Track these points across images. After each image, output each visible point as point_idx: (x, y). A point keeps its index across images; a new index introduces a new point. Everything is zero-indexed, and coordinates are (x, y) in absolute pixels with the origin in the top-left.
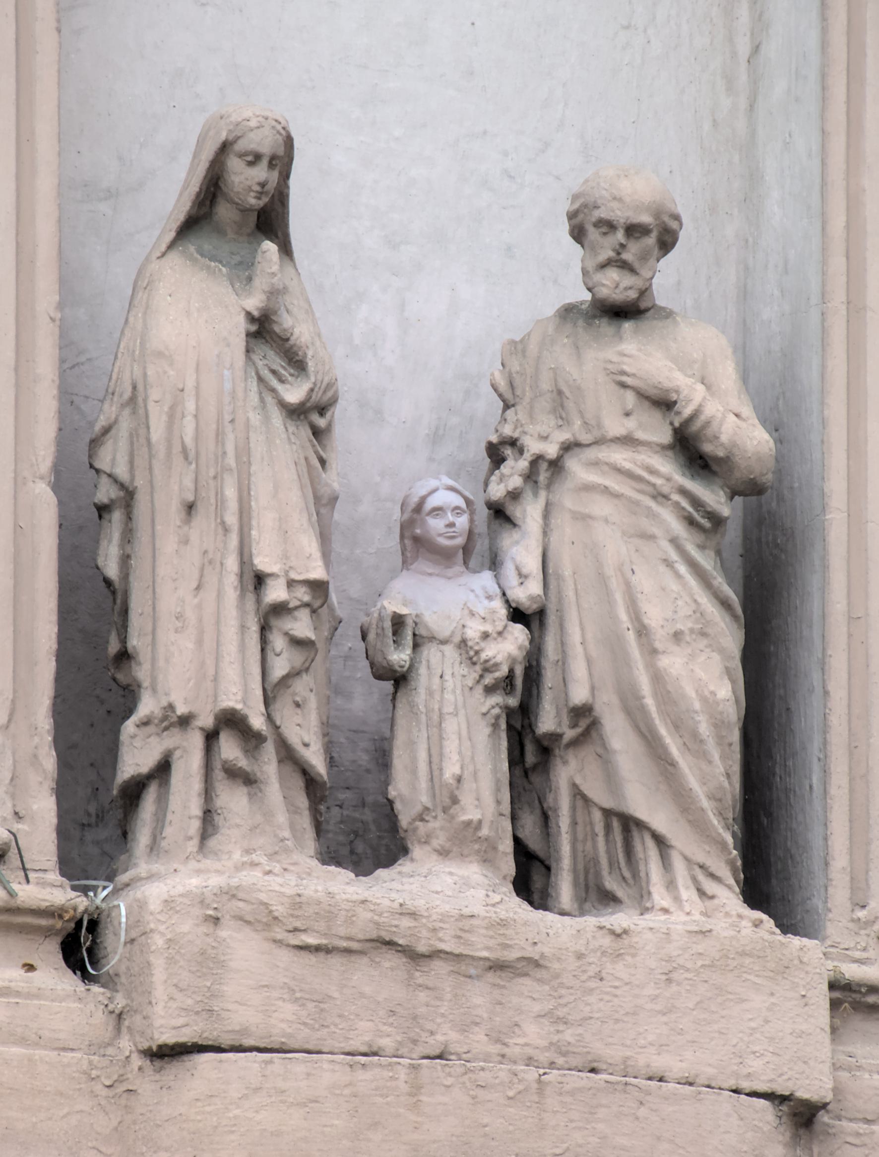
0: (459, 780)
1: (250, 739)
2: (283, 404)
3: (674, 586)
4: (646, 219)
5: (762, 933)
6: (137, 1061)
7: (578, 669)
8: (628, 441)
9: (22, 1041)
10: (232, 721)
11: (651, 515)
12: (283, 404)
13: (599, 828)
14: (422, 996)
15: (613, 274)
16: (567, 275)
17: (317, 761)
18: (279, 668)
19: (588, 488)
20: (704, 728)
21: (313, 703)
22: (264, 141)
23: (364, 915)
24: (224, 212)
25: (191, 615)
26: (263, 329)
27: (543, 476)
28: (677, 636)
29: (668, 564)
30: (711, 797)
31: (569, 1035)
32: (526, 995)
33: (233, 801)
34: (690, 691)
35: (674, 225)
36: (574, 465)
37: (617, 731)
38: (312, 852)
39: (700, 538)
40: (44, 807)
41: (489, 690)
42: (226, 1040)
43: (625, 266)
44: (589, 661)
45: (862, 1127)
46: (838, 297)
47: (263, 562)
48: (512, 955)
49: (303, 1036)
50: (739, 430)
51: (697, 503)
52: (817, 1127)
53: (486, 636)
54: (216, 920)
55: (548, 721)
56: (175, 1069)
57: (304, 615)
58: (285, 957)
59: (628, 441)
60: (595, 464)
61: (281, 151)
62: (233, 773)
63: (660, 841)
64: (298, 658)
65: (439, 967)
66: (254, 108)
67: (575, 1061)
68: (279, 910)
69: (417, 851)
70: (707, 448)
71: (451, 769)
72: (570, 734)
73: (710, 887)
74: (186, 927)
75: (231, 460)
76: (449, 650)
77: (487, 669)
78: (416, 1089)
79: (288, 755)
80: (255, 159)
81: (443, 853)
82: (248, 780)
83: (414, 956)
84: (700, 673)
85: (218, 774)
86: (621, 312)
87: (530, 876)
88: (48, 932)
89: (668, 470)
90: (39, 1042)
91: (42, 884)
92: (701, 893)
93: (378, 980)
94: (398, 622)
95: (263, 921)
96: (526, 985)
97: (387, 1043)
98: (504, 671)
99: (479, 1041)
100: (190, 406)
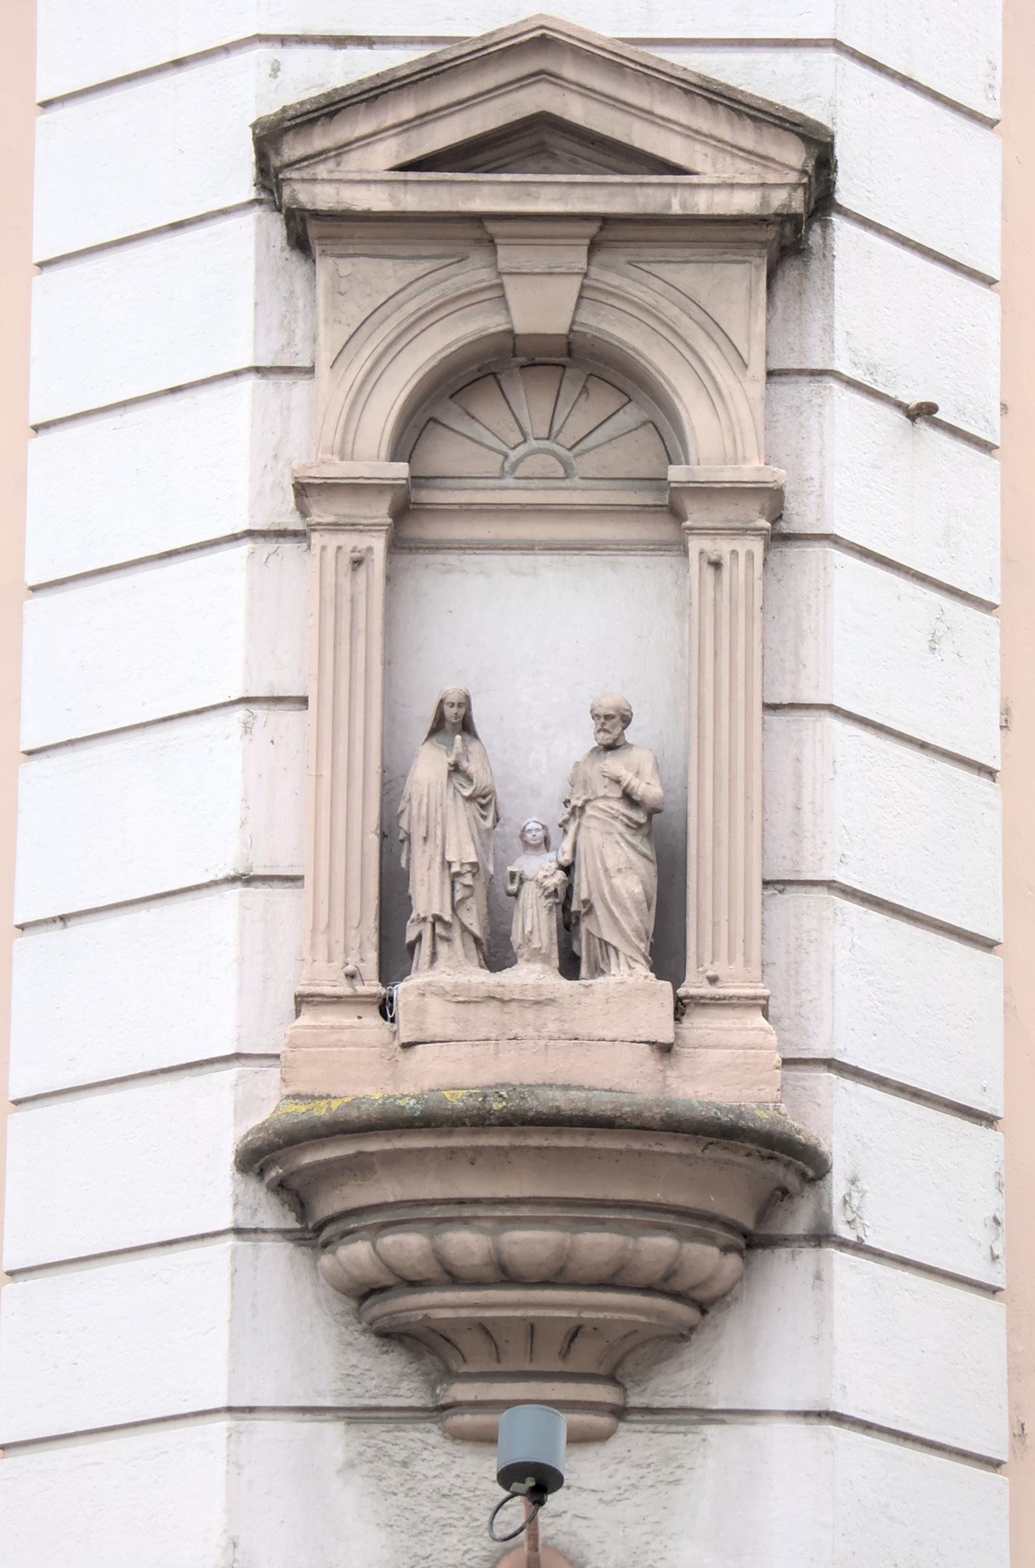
0: (531, 933)
1: (447, 925)
2: (463, 797)
3: (619, 851)
4: (611, 712)
5: (648, 981)
6: (399, 1049)
7: (584, 886)
8: (605, 797)
9: (356, 1045)
10: (438, 919)
11: (611, 825)
12: (463, 797)
13: (598, 945)
14: (507, 1016)
15: (602, 734)
16: (586, 737)
17: (477, 931)
18: (458, 897)
19: (590, 816)
20: (629, 904)
21: (474, 908)
22: (454, 698)
23: (483, 988)
24: (447, 726)
25: (426, 879)
26: (455, 769)
27: (577, 813)
28: (620, 870)
29: (618, 843)
30: (633, 930)
31: (566, 1026)
32: (549, 1012)
33: (442, 948)
34: (623, 891)
35: (627, 713)
36: (589, 810)
37: (599, 910)
38: (477, 961)
39: (633, 832)
40: (372, 956)
41: (547, 897)
42: (428, 1040)
43: (606, 731)
44: (589, 883)
45: (691, 1050)
46: (695, 735)
47: (448, 858)
48: (542, 998)
49: (459, 1036)
50: (649, 788)
51: (630, 819)
52: (673, 1052)
53: (546, 877)
54: (423, 995)
55: (574, 907)
56: (410, 1051)
57: (469, 876)
58: (452, 1006)
59: (605, 797)
60: (594, 807)
61: (463, 701)
62: (443, 938)
63: (615, 949)
64: (467, 892)
65: (513, 1004)
66: (451, 688)
67: (569, 1036)
68: (448, 989)
69: (519, 961)
70: (634, 797)
71: (528, 929)
72: (583, 911)
73: (633, 964)
74: (411, 998)
75: (439, 820)
76: (533, 884)
77: (546, 889)
78: (497, 1052)
79: (465, 929)
80: (453, 705)
81: (528, 961)
82: (448, 940)
83: (503, 1001)
84: (628, 883)
85: (437, 939)
86: (610, 747)
87: (570, 966)
88: (373, 1003)
89: (620, 807)
90: (363, 1045)
91: (369, 985)
92: (630, 967)
93: (489, 1012)
94: (513, 875)
95: (442, 993)
96: (549, 1008)
97: (493, 1035)
98: (552, 889)
99: (530, 1031)
100: (425, 800)
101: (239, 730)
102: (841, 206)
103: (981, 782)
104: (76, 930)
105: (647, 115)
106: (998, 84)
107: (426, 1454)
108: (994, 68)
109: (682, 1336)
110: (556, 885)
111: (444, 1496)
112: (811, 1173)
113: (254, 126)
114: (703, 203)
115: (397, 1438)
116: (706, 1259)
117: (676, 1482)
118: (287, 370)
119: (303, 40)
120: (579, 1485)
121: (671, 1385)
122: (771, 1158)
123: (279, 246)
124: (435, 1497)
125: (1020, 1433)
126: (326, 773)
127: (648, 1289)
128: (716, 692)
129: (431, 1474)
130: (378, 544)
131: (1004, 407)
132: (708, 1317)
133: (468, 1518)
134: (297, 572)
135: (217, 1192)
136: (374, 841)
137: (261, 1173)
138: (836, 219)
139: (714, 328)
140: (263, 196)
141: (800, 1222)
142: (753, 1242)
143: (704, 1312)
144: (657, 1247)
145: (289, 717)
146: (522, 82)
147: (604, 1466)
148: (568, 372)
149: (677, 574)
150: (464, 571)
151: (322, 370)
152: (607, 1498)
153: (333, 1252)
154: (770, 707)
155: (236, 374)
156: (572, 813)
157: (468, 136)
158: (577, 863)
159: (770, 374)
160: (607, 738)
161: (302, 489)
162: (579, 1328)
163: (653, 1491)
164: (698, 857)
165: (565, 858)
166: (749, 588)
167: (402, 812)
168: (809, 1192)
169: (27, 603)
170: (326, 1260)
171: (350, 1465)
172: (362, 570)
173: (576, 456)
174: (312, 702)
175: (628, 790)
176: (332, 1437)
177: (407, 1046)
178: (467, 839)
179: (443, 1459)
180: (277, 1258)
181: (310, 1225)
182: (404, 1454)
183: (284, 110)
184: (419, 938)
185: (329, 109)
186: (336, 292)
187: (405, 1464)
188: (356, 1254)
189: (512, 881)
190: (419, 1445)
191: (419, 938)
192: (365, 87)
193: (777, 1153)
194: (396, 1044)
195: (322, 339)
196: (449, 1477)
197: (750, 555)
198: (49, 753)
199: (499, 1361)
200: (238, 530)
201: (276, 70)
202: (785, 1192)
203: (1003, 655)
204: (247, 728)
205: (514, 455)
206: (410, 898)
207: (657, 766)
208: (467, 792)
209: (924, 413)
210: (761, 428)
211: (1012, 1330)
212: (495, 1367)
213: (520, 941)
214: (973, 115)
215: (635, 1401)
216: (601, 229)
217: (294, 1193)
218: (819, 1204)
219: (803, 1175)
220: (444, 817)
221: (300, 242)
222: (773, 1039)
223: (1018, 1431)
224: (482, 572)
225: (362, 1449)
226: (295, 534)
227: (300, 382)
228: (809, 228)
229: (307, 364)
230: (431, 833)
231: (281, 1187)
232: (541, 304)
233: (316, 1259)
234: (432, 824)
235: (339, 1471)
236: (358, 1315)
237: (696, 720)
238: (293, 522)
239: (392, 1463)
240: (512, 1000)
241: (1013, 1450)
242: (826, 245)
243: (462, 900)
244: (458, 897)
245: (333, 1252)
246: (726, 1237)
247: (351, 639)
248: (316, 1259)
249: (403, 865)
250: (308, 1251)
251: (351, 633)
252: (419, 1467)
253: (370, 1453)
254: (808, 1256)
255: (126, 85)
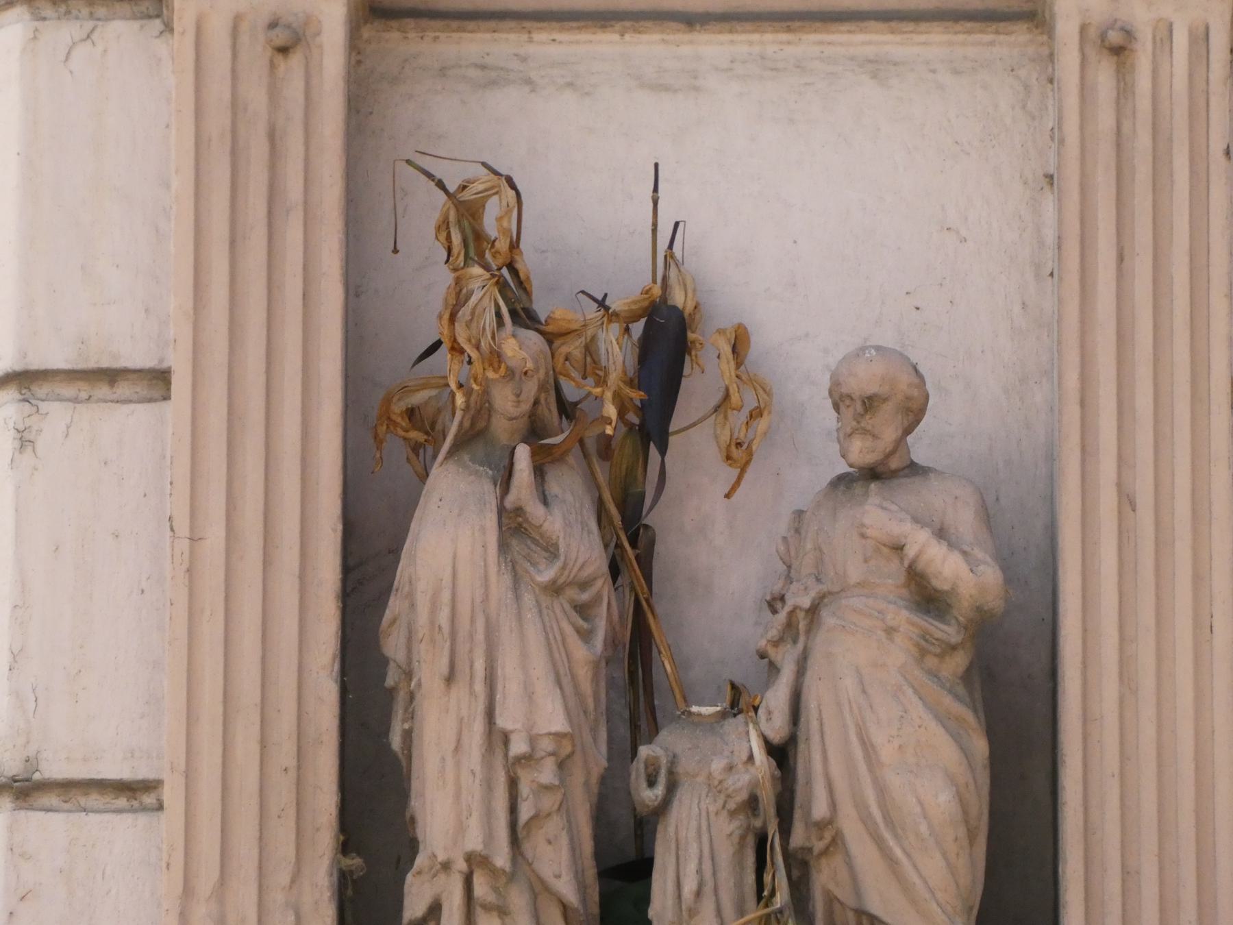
50: (967, 574)
71: (689, 887)
75: (480, 636)
85: (479, 910)
89: (903, 617)
98: (744, 796)
100: (446, 596)
105: (524, 655)
110: (755, 784)
126: (215, 536)
136: (326, 691)
145: (128, 424)
149: (1027, 87)
150: (529, 82)
156: (790, 625)
158: (801, 736)
160: (862, 452)
164: (1085, 720)
165: (777, 728)
167: (394, 621)
174: (181, 385)
175: (920, 566)
189: (651, 783)
206: (413, 820)
207: (987, 516)
208: (546, 575)
224: (570, 85)
230: (463, 666)
234: (463, 649)
244: (525, 812)
247: (270, 225)
249: (396, 741)
251: (270, 213)
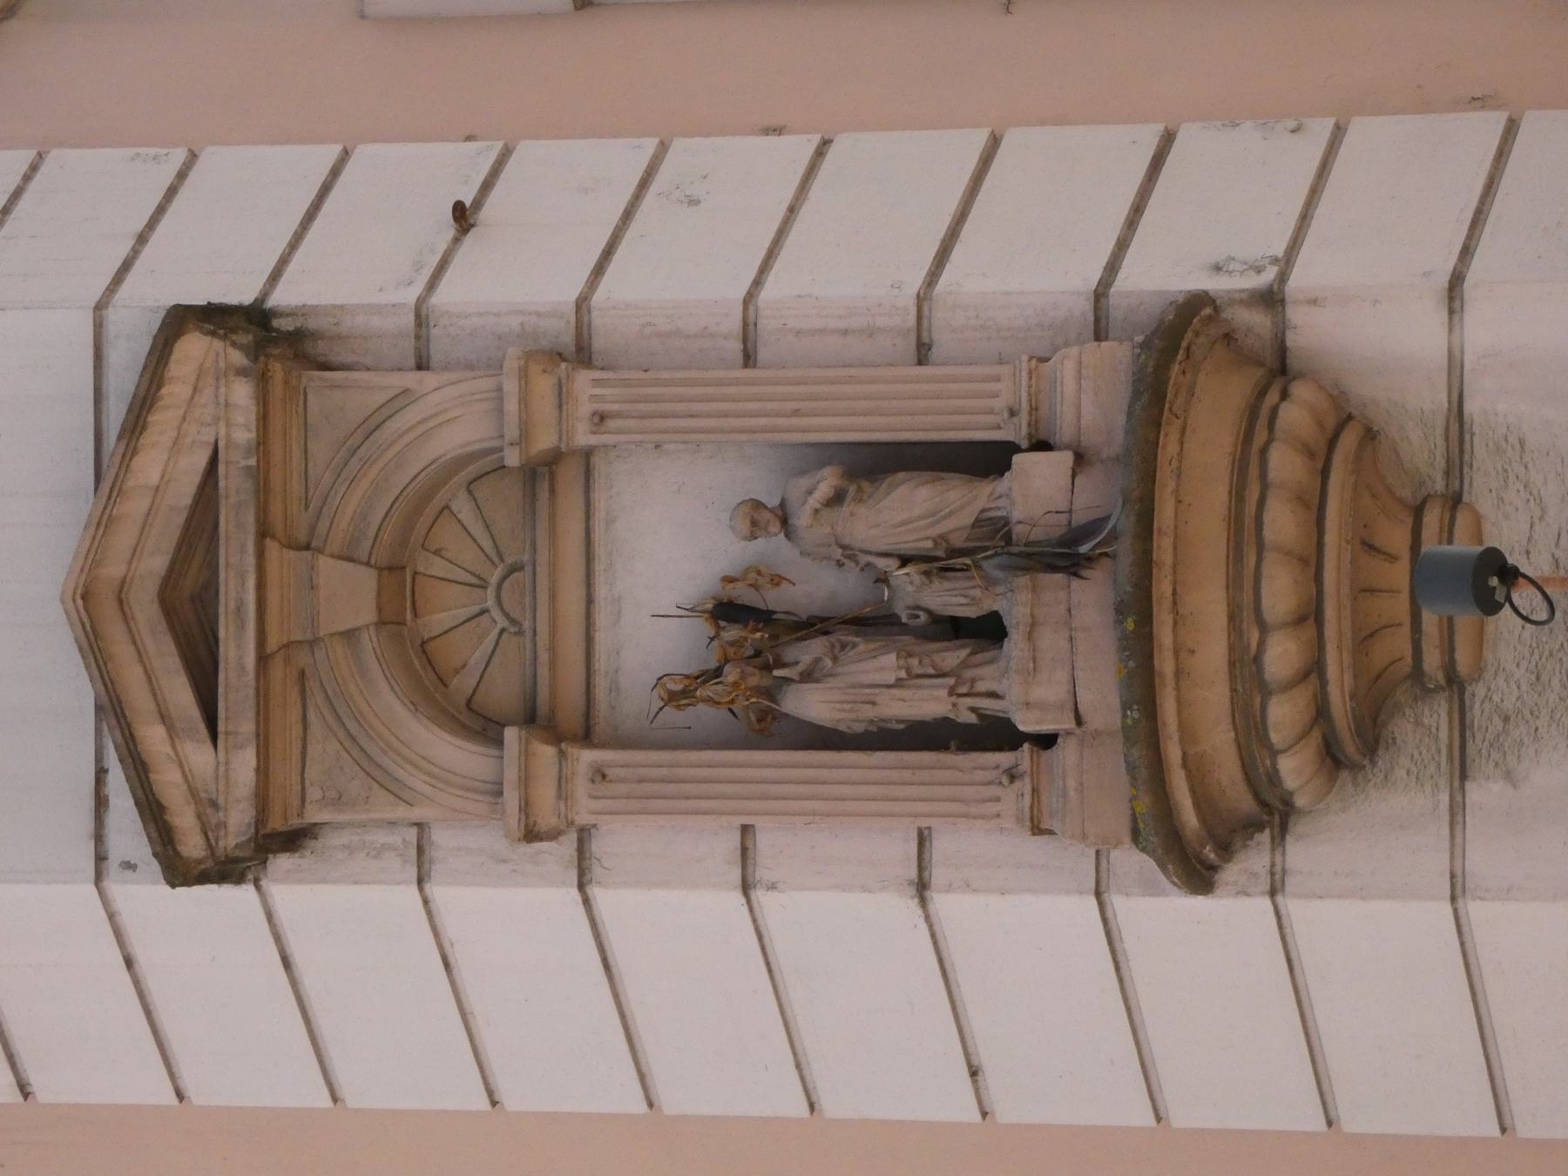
50: (827, 481)
71: (963, 600)
79: (964, 665)
82: (973, 681)
86: (785, 521)
89: (845, 510)
101: (772, 895)
102: (256, 300)
103: (833, 153)
104: (986, 1057)
106: (152, 151)
107: (1496, 698)
108: (138, 155)
109: (1370, 435)
111: (1538, 678)
112: (1208, 311)
113: (173, 886)
114: (244, 435)
115: (1480, 727)
116: (1297, 414)
117: (1522, 442)
118: (420, 850)
119: (99, 838)
120: (1524, 542)
121: (1420, 449)
122: (1188, 349)
123: (300, 861)
124: (1540, 688)
125: (1478, 102)
127: (1325, 473)
128: (725, 415)
129: (1516, 693)
130: (587, 757)
131: (469, 138)
132: (1355, 413)
133: (1561, 654)
134: (618, 841)
135: (1232, 916)
137: (1213, 868)
138: (271, 303)
139: (372, 426)
140: (250, 877)
141: (1257, 321)
142: (1279, 368)
143: (1350, 417)
144: (1285, 464)
146: (126, 618)
147: (1507, 517)
148: (421, 569)
151: (416, 814)
152: (1538, 513)
153: (1291, 794)
154: (749, 359)
155: (426, 902)
157: (182, 672)
159: (419, 367)
160: (775, 527)
161: (531, 835)
162: (1364, 543)
163: (1530, 466)
166: (626, 383)
168: (1226, 314)
169: (666, 1112)
170: (1300, 801)
171: (1509, 776)
172: (608, 771)
173: (502, 560)
174: (746, 820)
176: (1484, 793)
177: (1079, 721)
178: (876, 663)
179: (1501, 681)
180: (1304, 853)
181: (1266, 818)
182: (1497, 721)
183: (155, 855)
184: (973, 710)
185: (152, 811)
186: (338, 801)
187: (1506, 719)
188: (1294, 769)
189: (918, 617)
190: (1487, 706)
191: (973, 710)
192: (133, 774)
193: (1184, 344)
194: (1078, 731)
195: (388, 816)
196: (1520, 673)
197: (597, 382)
198: (810, 1086)
199: (1399, 625)
200: (579, 898)
201: (129, 866)
202: (1228, 337)
203: (708, 135)
204: (772, 887)
205: (502, 622)
207: (802, 472)
208: (828, 662)
209: (463, 216)
210: (469, 374)
211: (1378, 110)
212: (1406, 629)
213: (973, 609)
214: (182, 175)
215: (1440, 486)
216: (273, 537)
217: (1228, 836)
218: (1232, 302)
219: (1210, 317)
220: (853, 686)
221: (293, 840)
222: (1074, 351)
223: (1479, 103)
225: (1492, 764)
226: (581, 842)
227: (434, 838)
228: (277, 330)
229: (414, 831)
231: (1226, 850)
232: (348, 596)
233: (1299, 812)
235: (1515, 787)
236: (1355, 768)
237: (756, 436)
238: (568, 844)
239: (1505, 732)
240: (1033, 616)
241: (1499, 108)
242: (292, 313)
243: (933, 667)
245: (1291, 794)
246: (1272, 397)
248: (1299, 812)
249: (902, 726)
250: (1292, 819)
252: (1509, 705)
253: (1495, 755)
254: (1296, 315)
255: (155, 1015)
